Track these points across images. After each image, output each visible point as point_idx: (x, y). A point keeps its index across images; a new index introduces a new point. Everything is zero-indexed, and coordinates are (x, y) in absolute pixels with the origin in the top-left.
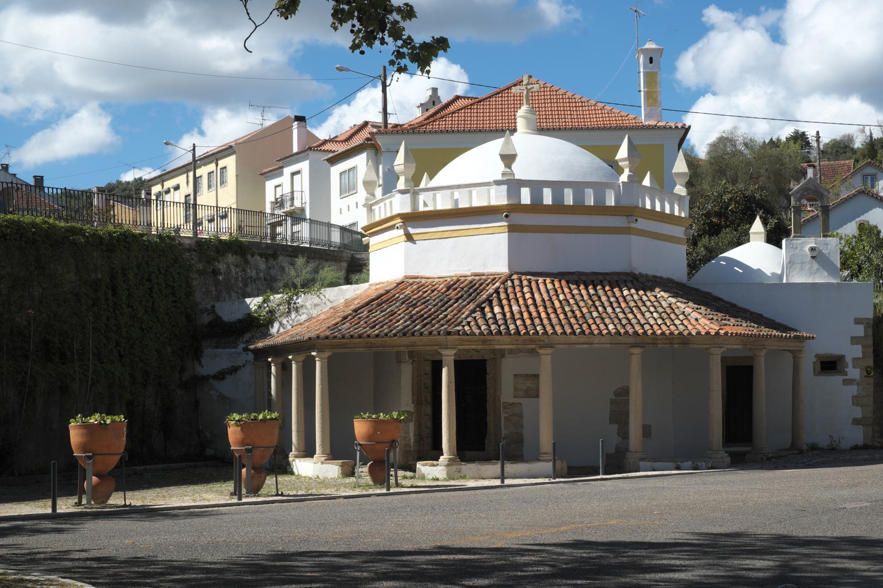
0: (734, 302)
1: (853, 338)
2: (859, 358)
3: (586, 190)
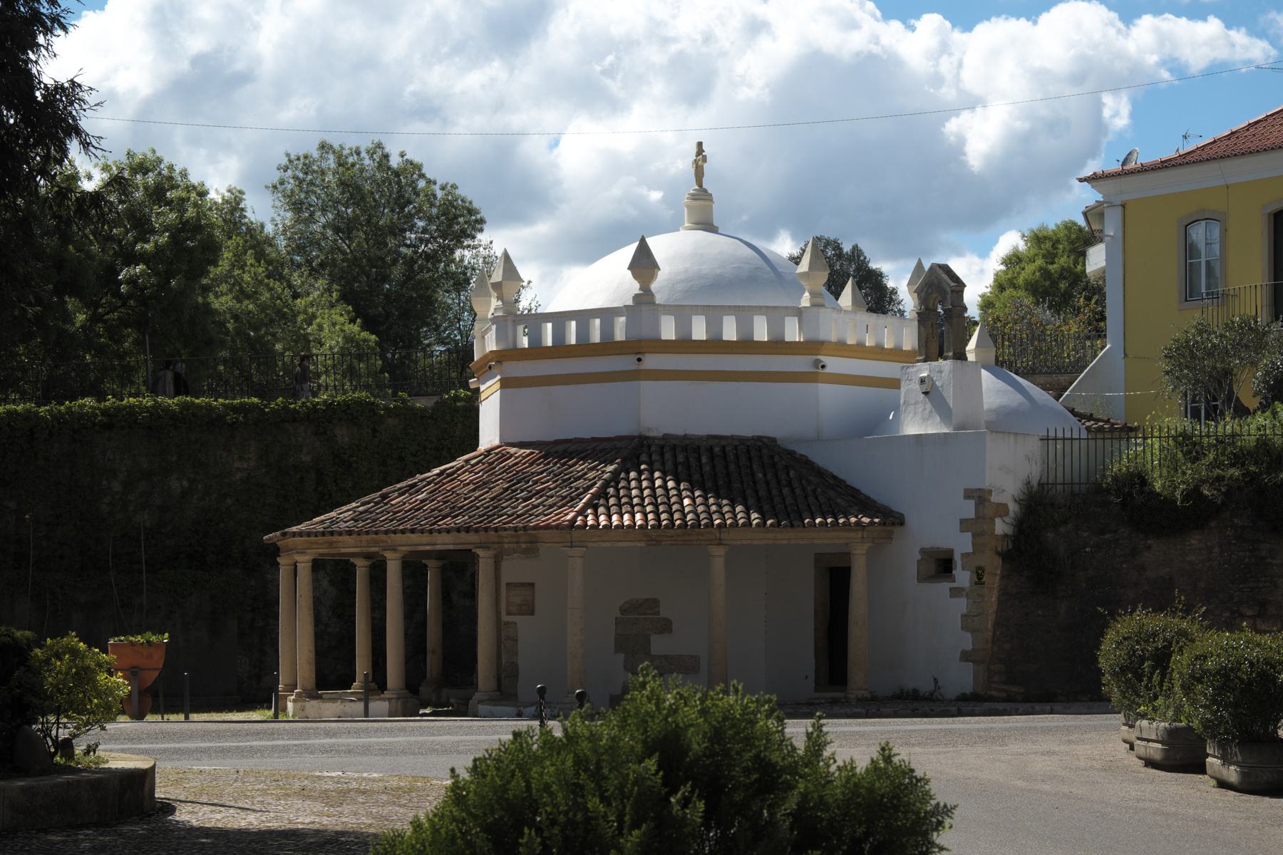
0: (842, 476)
1: (962, 521)
2: (968, 554)
3: (694, 318)
